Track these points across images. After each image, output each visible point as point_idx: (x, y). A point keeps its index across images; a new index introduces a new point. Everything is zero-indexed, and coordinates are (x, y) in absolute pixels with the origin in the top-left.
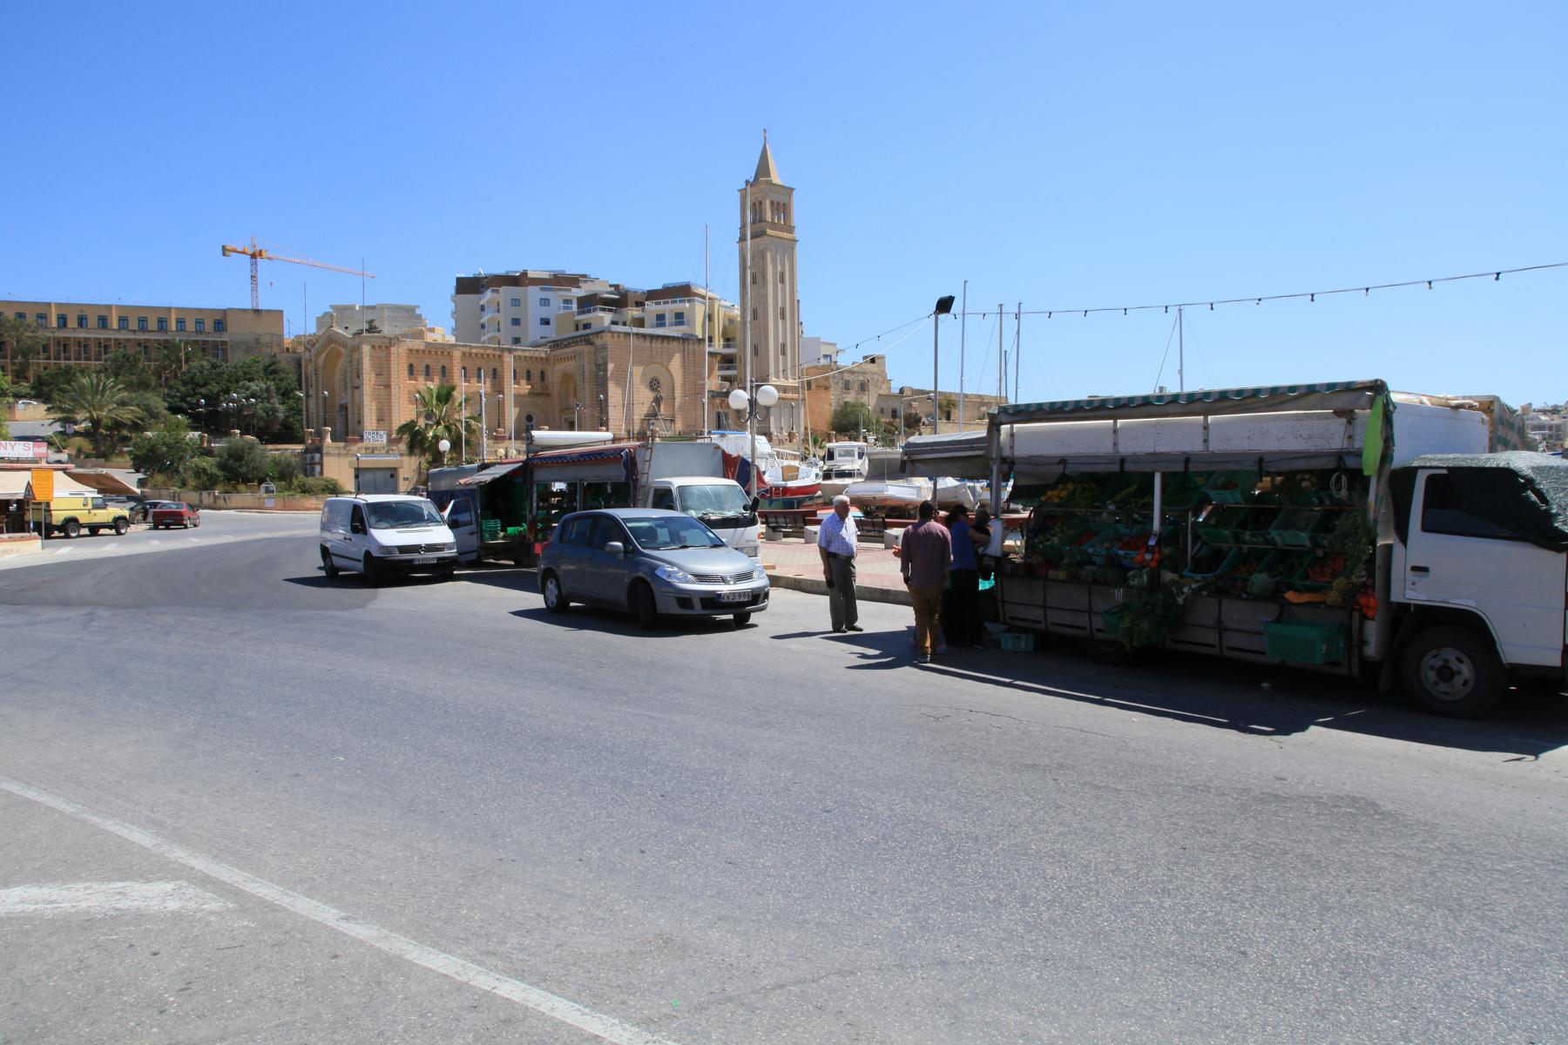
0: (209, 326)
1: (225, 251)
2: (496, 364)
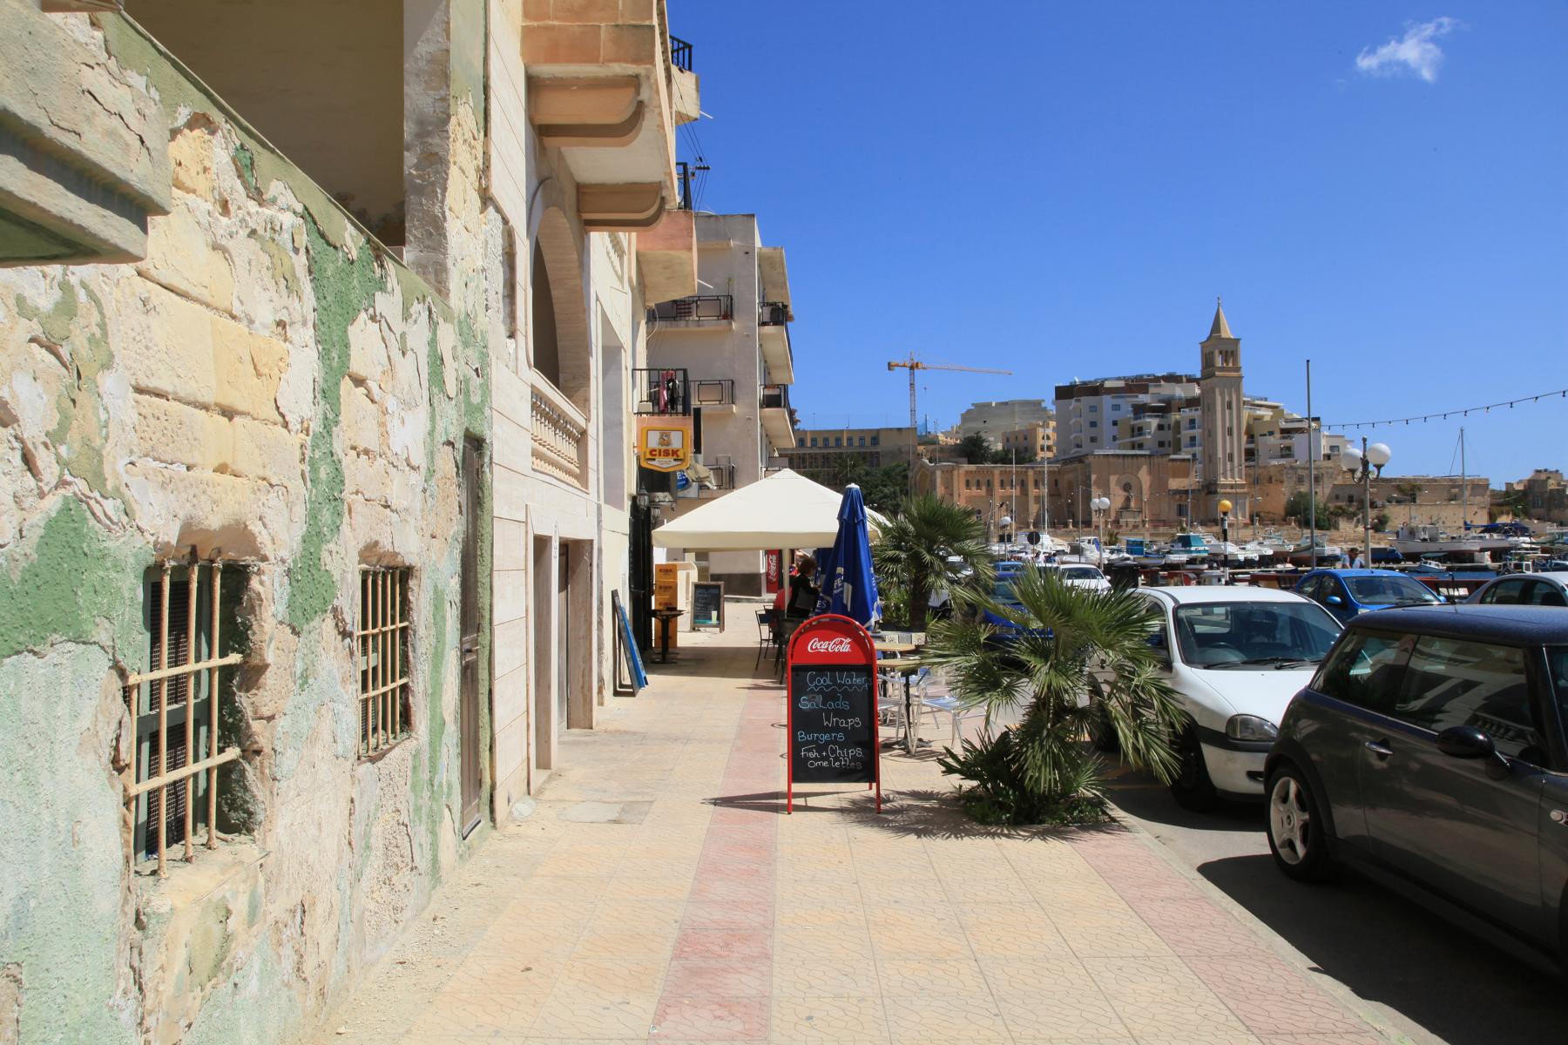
0: (868, 442)
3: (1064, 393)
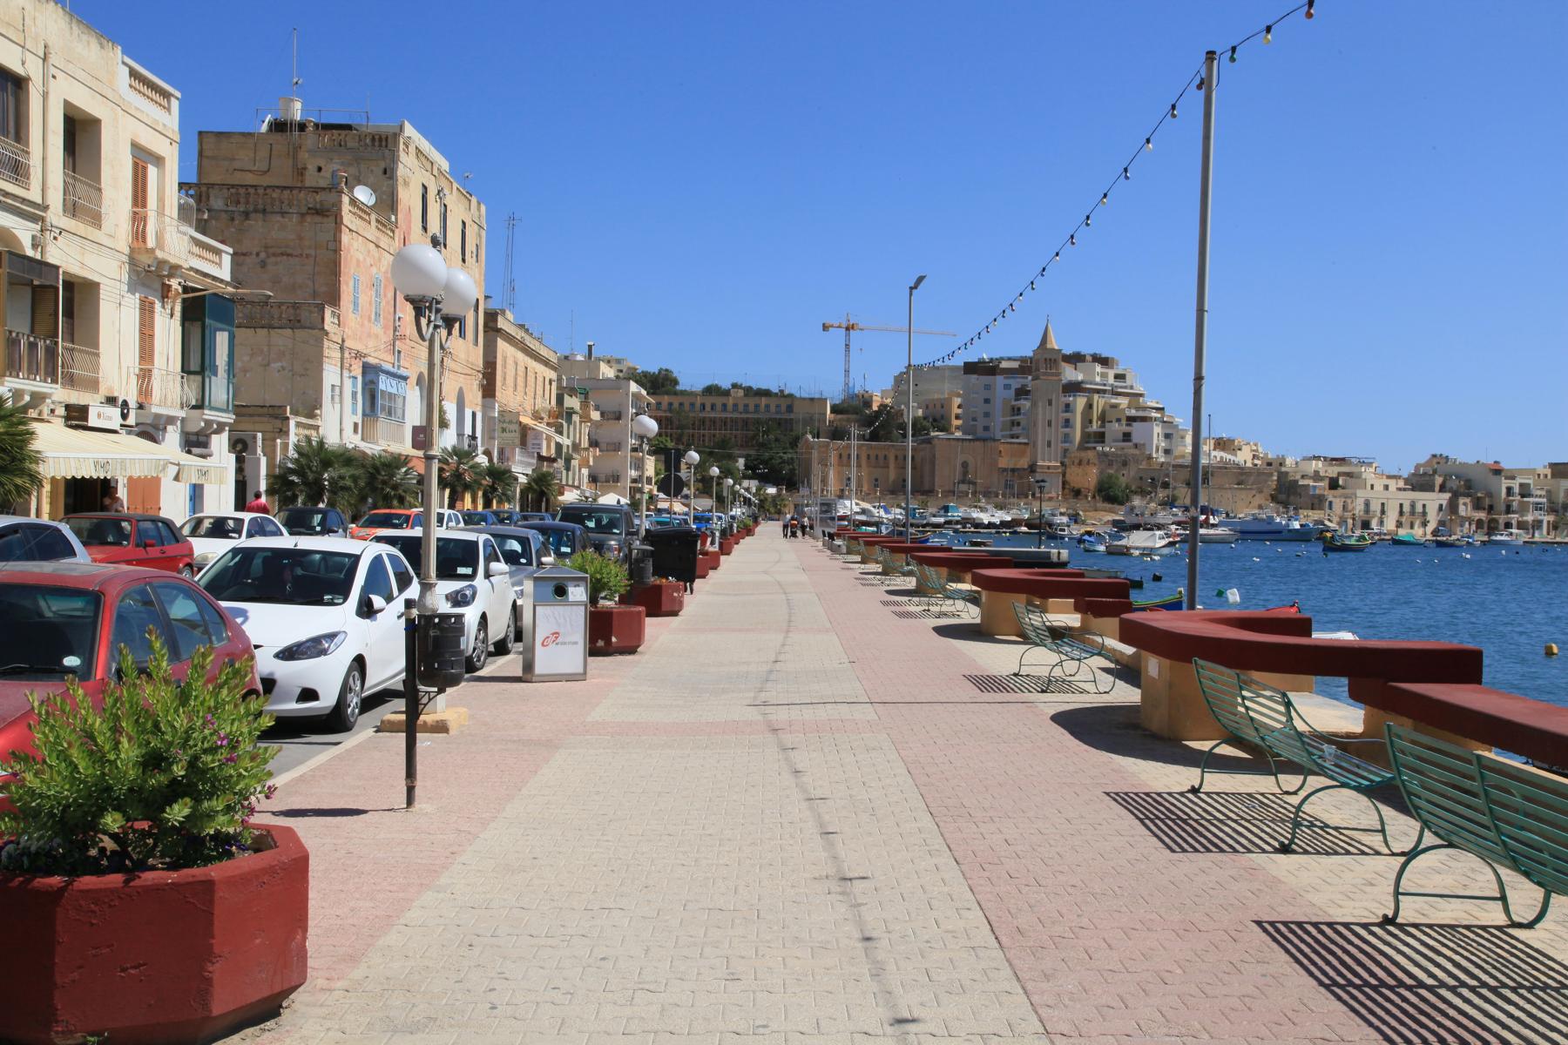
1: (825, 328)
3: (970, 368)
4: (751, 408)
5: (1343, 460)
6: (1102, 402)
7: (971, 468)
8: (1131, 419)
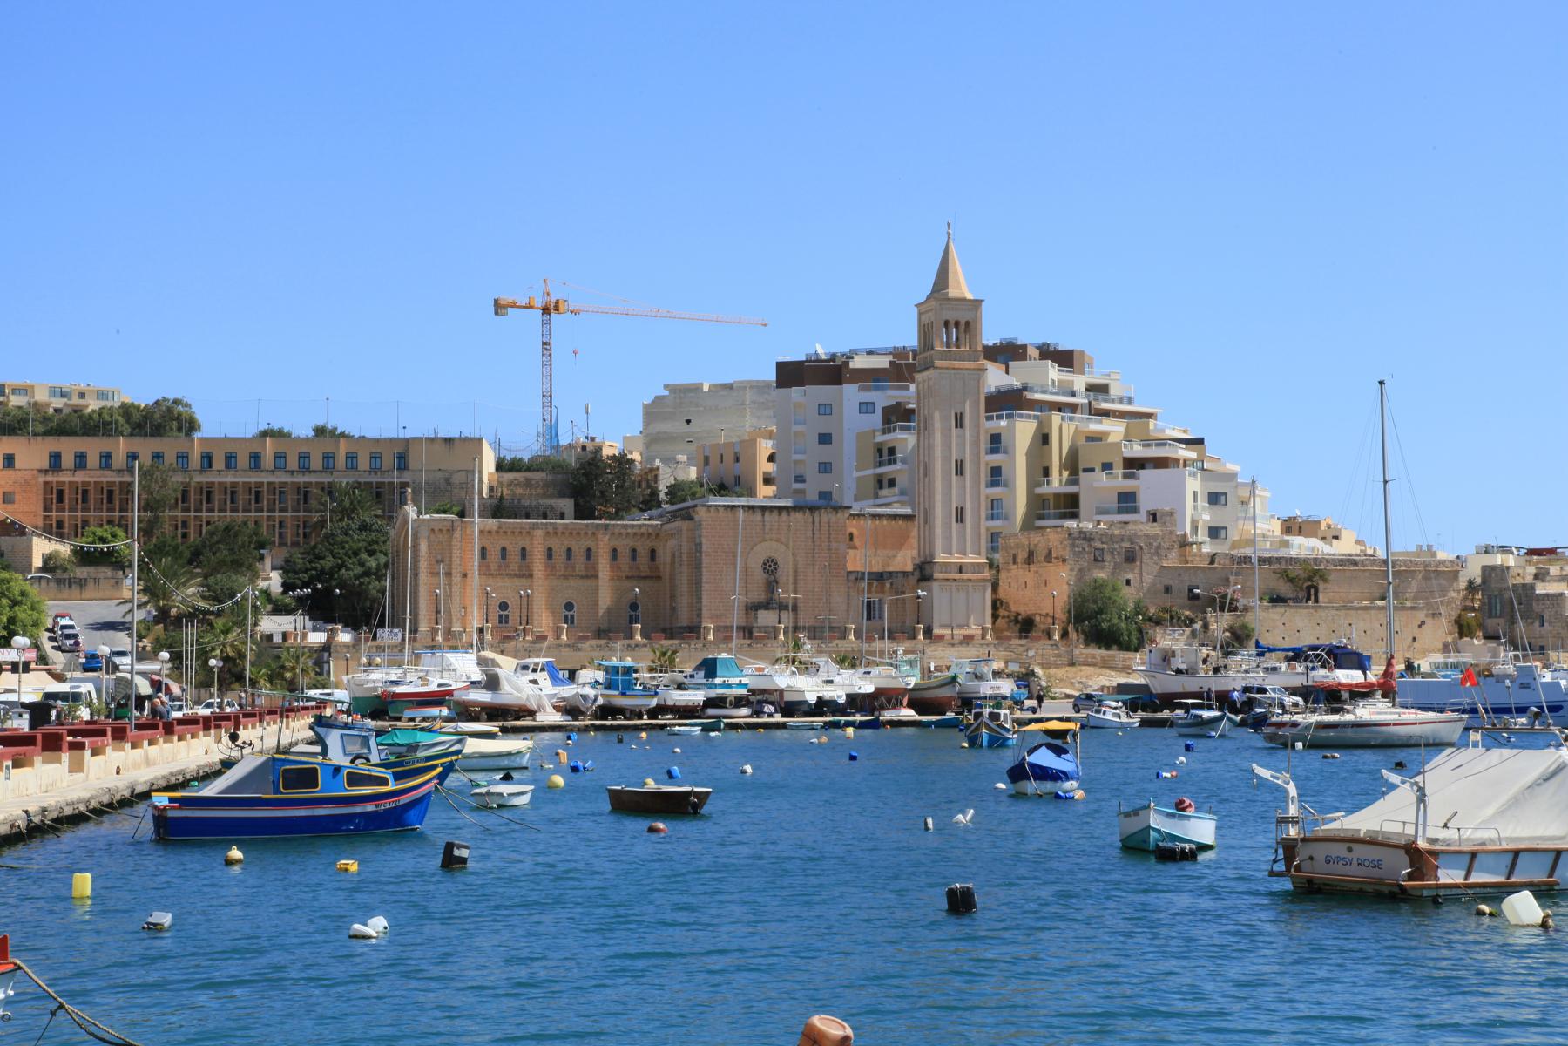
0: (387, 461)
1: (499, 308)
2: (590, 543)
3: (790, 374)
4: (316, 462)
5: (1552, 551)
6: (1069, 429)
7: (785, 573)
8: (1135, 465)
